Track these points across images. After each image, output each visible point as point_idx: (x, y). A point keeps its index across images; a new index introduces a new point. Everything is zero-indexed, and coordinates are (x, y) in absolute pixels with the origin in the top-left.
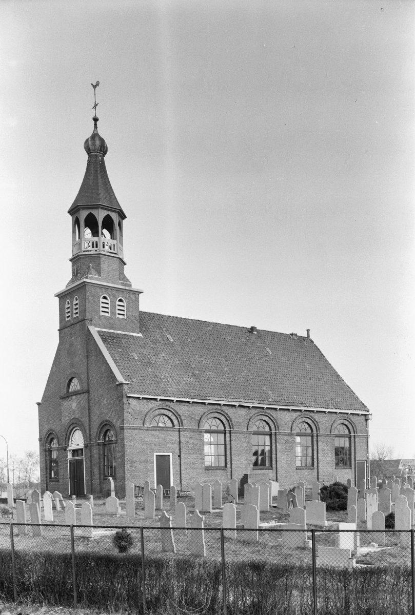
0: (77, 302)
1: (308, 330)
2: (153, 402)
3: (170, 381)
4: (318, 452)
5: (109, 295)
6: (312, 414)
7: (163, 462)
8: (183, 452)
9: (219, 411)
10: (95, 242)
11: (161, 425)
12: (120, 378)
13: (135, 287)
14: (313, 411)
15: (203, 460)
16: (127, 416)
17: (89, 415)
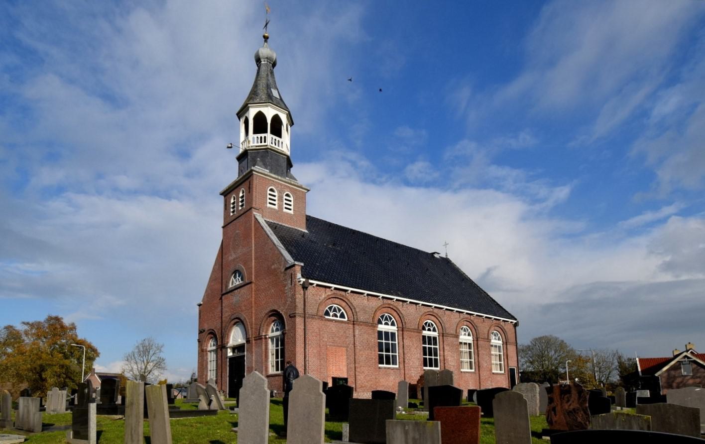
9: (391, 307)
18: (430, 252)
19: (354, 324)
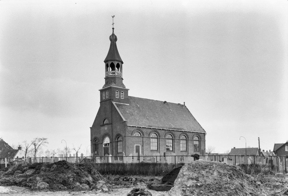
0: (108, 93)
1: (184, 103)
2: (135, 127)
3: (140, 120)
6: (186, 133)
7: (138, 148)
8: (144, 145)
10: (114, 72)
11: (137, 135)
12: (124, 120)
13: (127, 88)
14: (187, 132)
15: (150, 147)
16: (127, 133)
17: (112, 132)
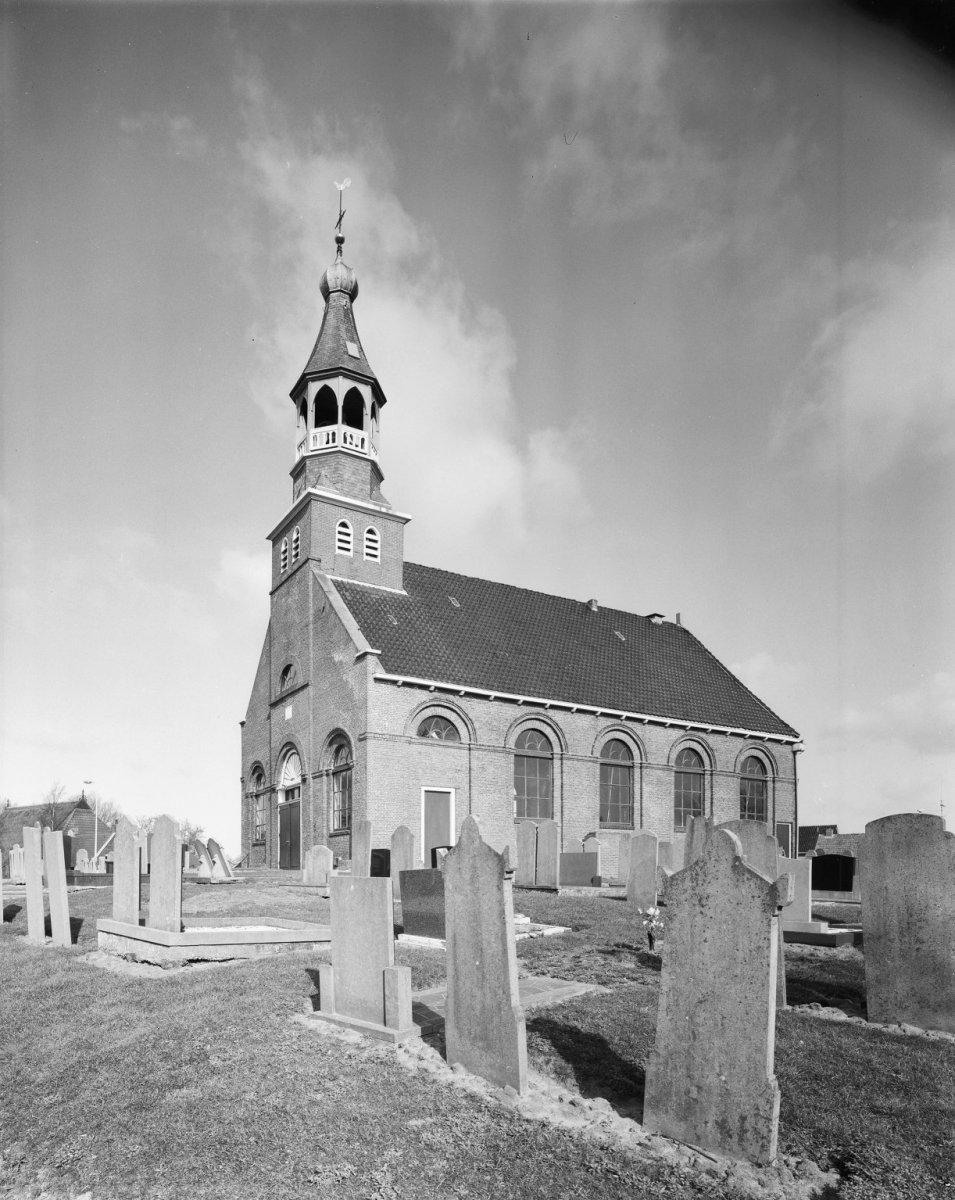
4: (712, 803)
5: (351, 519)
9: (542, 718)
10: (330, 433)
18: (644, 613)
19: (470, 749)
